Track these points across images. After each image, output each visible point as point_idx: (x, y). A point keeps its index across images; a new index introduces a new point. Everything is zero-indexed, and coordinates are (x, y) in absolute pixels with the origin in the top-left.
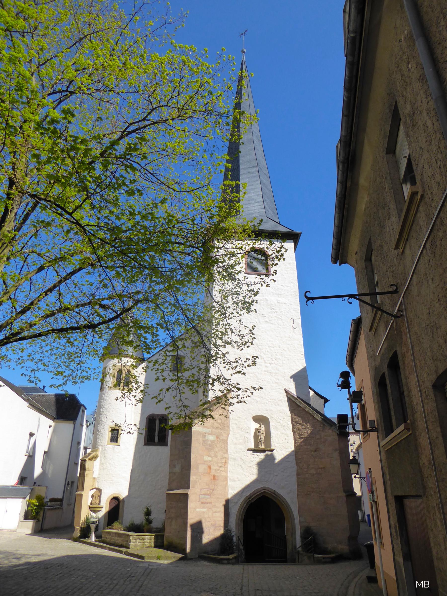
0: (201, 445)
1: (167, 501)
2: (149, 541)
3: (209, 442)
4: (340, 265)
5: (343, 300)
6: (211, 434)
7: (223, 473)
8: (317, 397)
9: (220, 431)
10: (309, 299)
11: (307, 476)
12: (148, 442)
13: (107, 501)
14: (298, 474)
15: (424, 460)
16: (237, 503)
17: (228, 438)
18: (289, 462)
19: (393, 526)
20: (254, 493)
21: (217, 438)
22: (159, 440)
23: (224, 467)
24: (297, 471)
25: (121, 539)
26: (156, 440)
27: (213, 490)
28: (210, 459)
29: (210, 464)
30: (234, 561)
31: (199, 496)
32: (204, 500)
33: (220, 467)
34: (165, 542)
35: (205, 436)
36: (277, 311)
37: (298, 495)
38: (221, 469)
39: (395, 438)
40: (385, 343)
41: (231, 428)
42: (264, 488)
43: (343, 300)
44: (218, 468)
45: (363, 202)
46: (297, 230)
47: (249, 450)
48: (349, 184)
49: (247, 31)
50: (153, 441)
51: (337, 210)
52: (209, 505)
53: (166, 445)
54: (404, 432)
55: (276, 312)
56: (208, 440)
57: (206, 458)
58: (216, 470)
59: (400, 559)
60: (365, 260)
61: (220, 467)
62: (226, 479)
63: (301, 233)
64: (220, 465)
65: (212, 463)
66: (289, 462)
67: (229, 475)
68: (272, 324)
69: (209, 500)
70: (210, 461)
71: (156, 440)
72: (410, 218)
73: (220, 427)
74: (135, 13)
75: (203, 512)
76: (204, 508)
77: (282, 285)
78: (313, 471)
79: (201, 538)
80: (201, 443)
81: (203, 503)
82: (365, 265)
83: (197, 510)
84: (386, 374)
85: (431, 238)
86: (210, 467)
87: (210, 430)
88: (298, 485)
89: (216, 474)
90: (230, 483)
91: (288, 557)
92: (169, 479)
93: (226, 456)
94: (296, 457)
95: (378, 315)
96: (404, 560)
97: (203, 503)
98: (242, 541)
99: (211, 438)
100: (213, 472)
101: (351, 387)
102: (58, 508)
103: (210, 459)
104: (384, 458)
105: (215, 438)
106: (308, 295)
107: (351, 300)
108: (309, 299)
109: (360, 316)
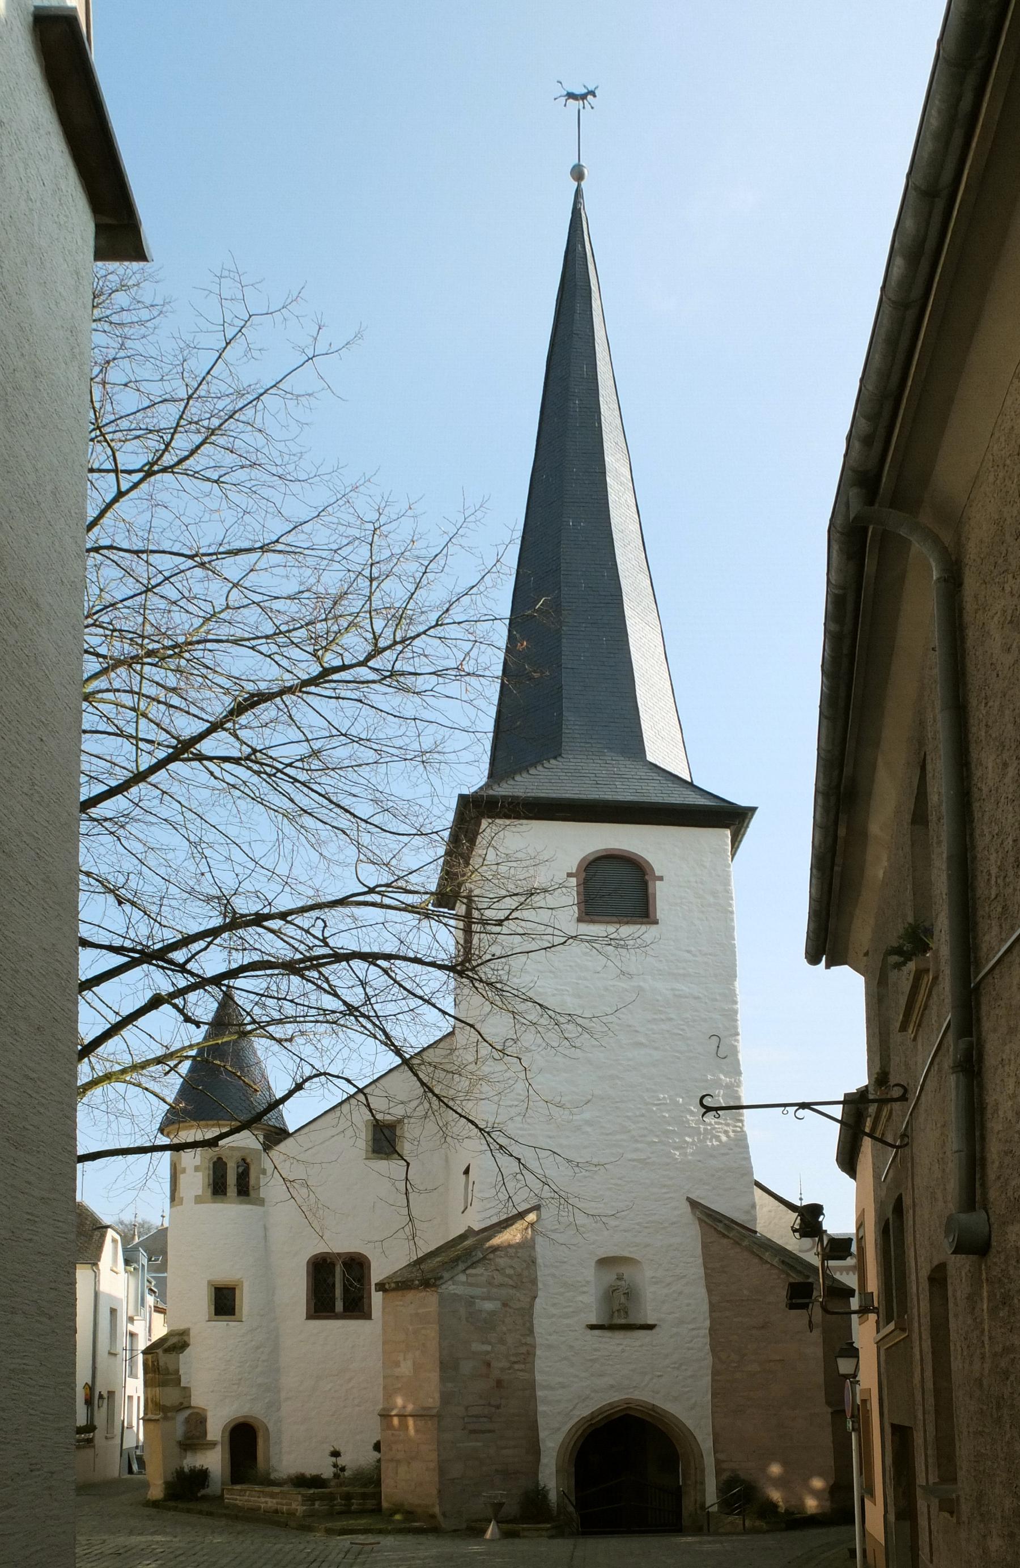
4: (828, 967)
6: (488, 1298)
7: (521, 1374)
8: (783, 1207)
9: (512, 1291)
10: (708, 1109)
13: (223, 1431)
17: (532, 1306)
19: (888, 1469)
20: (601, 1411)
21: (505, 1305)
22: (346, 1309)
23: (524, 1363)
24: (713, 1366)
25: (275, 1501)
26: (339, 1306)
27: (498, 1407)
28: (489, 1348)
29: (488, 1357)
31: (463, 1418)
33: (515, 1363)
34: (385, 1505)
36: (673, 1016)
38: (516, 1366)
39: (886, 1340)
40: (891, 1171)
41: (540, 1285)
42: (627, 1401)
44: (507, 1365)
45: (879, 864)
46: (741, 800)
47: (592, 1327)
48: (842, 832)
49: (593, 93)
50: (332, 1309)
51: (814, 871)
53: (368, 1316)
54: (896, 1333)
55: (670, 1019)
57: (477, 1347)
58: (502, 1370)
59: (892, 1518)
61: (515, 1363)
62: (532, 1386)
63: (753, 810)
64: (513, 1359)
65: (493, 1355)
68: (656, 1049)
70: (488, 1353)
71: (339, 1306)
72: (920, 999)
73: (511, 1282)
74: (227, 344)
77: (689, 952)
79: (75, 1031)
81: (473, 1432)
85: (937, 1060)
86: (489, 1365)
87: (485, 1290)
90: (539, 1393)
91: (686, 1521)
93: (529, 1340)
95: (884, 1114)
96: (896, 1519)
97: (473, 1432)
99: (489, 1306)
103: (489, 1348)
104: (883, 1358)
106: (707, 1102)
107: (802, 1113)
108: (708, 1109)
109: (866, 1086)
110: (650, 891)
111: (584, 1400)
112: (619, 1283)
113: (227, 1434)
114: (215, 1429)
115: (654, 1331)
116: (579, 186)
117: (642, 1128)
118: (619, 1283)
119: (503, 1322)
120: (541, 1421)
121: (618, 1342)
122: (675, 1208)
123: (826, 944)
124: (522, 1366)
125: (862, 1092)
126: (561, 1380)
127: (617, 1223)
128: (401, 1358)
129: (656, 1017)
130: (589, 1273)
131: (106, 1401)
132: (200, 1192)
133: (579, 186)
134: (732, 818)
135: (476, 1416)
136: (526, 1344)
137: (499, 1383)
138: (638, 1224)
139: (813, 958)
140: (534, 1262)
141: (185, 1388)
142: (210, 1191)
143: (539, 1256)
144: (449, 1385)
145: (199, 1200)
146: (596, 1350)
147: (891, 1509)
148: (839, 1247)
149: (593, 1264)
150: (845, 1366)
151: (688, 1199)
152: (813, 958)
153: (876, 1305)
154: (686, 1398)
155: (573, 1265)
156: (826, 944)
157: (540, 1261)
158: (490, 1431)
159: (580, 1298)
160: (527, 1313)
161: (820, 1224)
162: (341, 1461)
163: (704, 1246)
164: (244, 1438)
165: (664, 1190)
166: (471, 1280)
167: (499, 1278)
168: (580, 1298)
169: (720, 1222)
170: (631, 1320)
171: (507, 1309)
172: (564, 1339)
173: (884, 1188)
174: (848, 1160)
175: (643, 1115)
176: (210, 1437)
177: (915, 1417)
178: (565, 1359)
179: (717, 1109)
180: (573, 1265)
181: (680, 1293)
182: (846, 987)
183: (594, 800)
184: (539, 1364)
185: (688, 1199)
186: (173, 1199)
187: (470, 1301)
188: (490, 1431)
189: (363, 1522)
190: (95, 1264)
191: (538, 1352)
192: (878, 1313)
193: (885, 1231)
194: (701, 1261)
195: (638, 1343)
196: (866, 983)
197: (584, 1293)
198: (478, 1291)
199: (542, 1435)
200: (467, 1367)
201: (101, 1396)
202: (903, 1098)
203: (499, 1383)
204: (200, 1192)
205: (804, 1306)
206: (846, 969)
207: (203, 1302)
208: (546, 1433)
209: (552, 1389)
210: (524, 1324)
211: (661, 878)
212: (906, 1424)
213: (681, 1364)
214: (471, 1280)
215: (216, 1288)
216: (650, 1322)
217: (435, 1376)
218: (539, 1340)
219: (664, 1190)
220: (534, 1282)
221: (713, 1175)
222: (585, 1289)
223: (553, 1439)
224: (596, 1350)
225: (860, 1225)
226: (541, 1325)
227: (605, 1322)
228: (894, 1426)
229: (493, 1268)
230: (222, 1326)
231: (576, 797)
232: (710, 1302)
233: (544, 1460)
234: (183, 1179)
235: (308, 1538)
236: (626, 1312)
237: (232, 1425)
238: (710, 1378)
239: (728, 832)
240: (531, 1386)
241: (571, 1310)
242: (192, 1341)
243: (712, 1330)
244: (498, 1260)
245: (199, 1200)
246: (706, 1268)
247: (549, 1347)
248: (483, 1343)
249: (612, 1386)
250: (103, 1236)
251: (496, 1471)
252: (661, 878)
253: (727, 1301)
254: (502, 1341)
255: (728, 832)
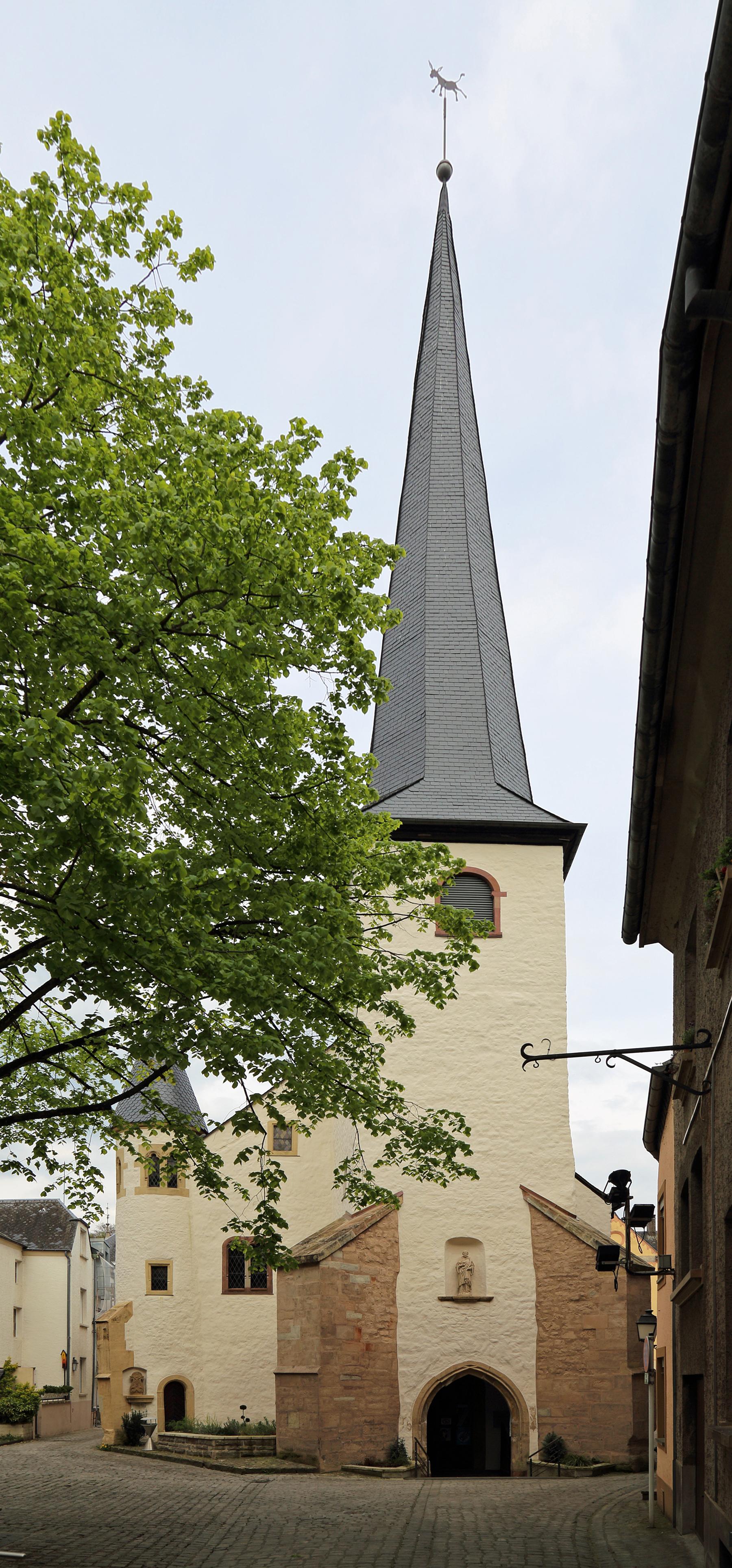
0: (340, 1293)
1: (277, 1387)
2: (247, 1447)
3: (357, 1287)
4: (641, 946)
5: (598, 1060)
6: (360, 1273)
7: (386, 1339)
9: (378, 1267)
10: (529, 1059)
11: (558, 1342)
12: (230, 1287)
13: (159, 1389)
14: (540, 1340)
15: (709, 1326)
16: (415, 1387)
17: (395, 1280)
18: (521, 1319)
21: (373, 1279)
22: (253, 1284)
28: (360, 1316)
30: (406, 1475)
32: (350, 1384)
33: (381, 1329)
34: (279, 1449)
35: (347, 1278)
37: (537, 1374)
38: (382, 1333)
43: (598, 1060)
44: (375, 1331)
46: (574, 819)
47: (442, 1299)
48: (659, 781)
52: (359, 1390)
53: (271, 1293)
56: (354, 1284)
57: (351, 1315)
58: (371, 1335)
59: (680, 1463)
60: (686, 949)
61: (381, 1329)
62: (393, 1350)
63: (583, 827)
64: (380, 1326)
65: (363, 1322)
66: (521, 1319)
67: (399, 1342)
68: (498, 1052)
69: (358, 1384)
70: (359, 1320)
75: (349, 1403)
76: (349, 1396)
77: (526, 962)
78: (571, 1335)
80: (340, 1290)
81: (346, 1388)
82: (686, 959)
83: (335, 1399)
84: (690, 1180)
86: (360, 1330)
87: (357, 1265)
88: (539, 1359)
89: (372, 1341)
92: (279, 1350)
94: (538, 1310)
96: (684, 1463)
97: (346, 1388)
98: (425, 1446)
99: (360, 1279)
100: (366, 1338)
101: (632, 1197)
102: (62, 1403)
103: (360, 1316)
105: (369, 1280)
106: (527, 1051)
107: (613, 1061)
108: (529, 1059)
110: (496, 906)
111: (435, 1362)
112: (465, 1261)
113: (162, 1391)
114: (153, 1387)
115: (491, 1303)
116: (444, 187)
117: (485, 1124)
118: (465, 1261)
119: (372, 1294)
120: (401, 1380)
121: (463, 1312)
122: (511, 1195)
123: (639, 926)
124: (387, 1333)
125: (668, 1065)
126: (417, 1344)
127: (463, 1208)
128: (291, 1324)
129: (498, 1022)
130: (441, 1251)
131: (79, 1365)
132: (138, 1185)
133: (444, 187)
134: (566, 836)
135: (350, 1375)
136: (390, 1313)
137: (368, 1347)
138: (480, 1209)
139: (628, 938)
140: (397, 1242)
141: (129, 1352)
142: (146, 1183)
143: (400, 1236)
144: (328, 1347)
145: (138, 1191)
146: (445, 1319)
147: (680, 1455)
148: (641, 1215)
149: (444, 1243)
150: (644, 1331)
151: (522, 1187)
152: (628, 938)
153: (673, 1267)
154: (518, 1369)
155: (428, 1245)
156: (639, 926)
157: (401, 1241)
158: (360, 1388)
159: (433, 1274)
160: (392, 1286)
161: (628, 1190)
162: (247, 1414)
163: (534, 1228)
164: (175, 1393)
165: (502, 1179)
166: (346, 1256)
167: (369, 1256)
168: (433, 1274)
169: (546, 1207)
170: (475, 1294)
171: (375, 1282)
172: (420, 1309)
173: (685, 1152)
174: (653, 1141)
175: (486, 1112)
176: (149, 1394)
177: (706, 1364)
178: (420, 1326)
179: (536, 1058)
180: (428, 1245)
181: (513, 1270)
182: (659, 959)
183: (450, 821)
184: (400, 1331)
185: (522, 1187)
186: (118, 1191)
187: (346, 1275)
188: (360, 1388)
189: (261, 1463)
190: (69, 1252)
191: (399, 1321)
192: (674, 1275)
193: (683, 1195)
194: (530, 1241)
195: (478, 1313)
196: (675, 958)
197: (437, 1269)
198: (351, 1267)
199: (402, 1391)
200: (342, 1332)
201: (74, 1362)
202: (707, 1044)
203: (368, 1347)
204: (138, 1185)
205: (611, 1268)
206: (657, 946)
207: (143, 1278)
208: (405, 1390)
209: (411, 1352)
210: (389, 1296)
211: (505, 894)
212: (697, 1372)
213: (513, 1332)
214: (346, 1256)
215: (152, 1267)
216: (489, 1295)
217: (316, 1340)
218: (400, 1310)
219: (502, 1179)
220: (397, 1259)
221: (542, 1166)
222: (437, 1266)
223: (411, 1394)
224: (445, 1319)
225: (661, 1198)
226: (401, 1296)
227: (452, 1294)
228: (685, 1378)
229: (364, 1246)
230: (158, 1298)
231: (435, 817)
232: (537, 1279)
233: (403, 1414)
234: (125, 1173)
235: (218, 1477)
236: (470, 1286)
237: (166, 1382)
238: (535, 1344)
239: (560, 849)
240: (393, 1351)
241: (426, 1284)
242: (134, 1312)
243: (538, 1304)
244: (368, 1240)
245: (138, 1191)
246: (534, 1248)
247: (409, 1316)
248: (356, 1312)
249: (457, 1351)
250: (74, 1228)
251: (365, 1421)
252: (505, 894)
253: (551, 1277)
254: (371, 1310)
255: (560, 849)
